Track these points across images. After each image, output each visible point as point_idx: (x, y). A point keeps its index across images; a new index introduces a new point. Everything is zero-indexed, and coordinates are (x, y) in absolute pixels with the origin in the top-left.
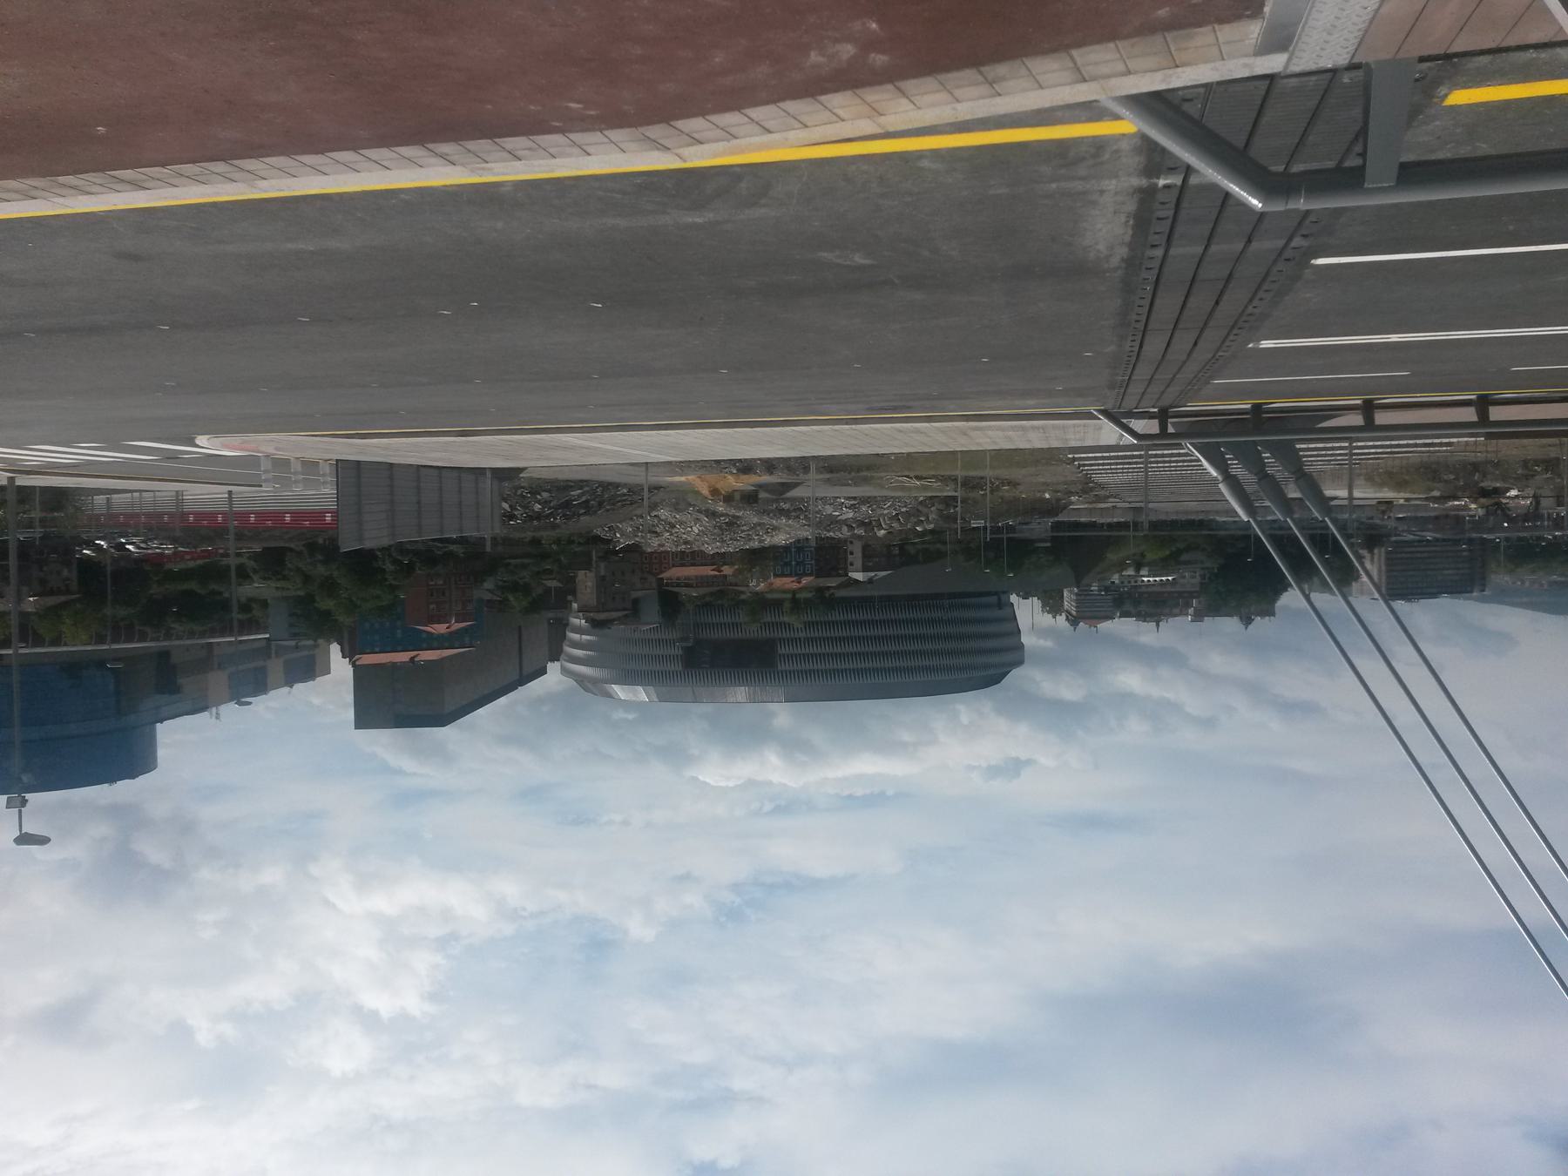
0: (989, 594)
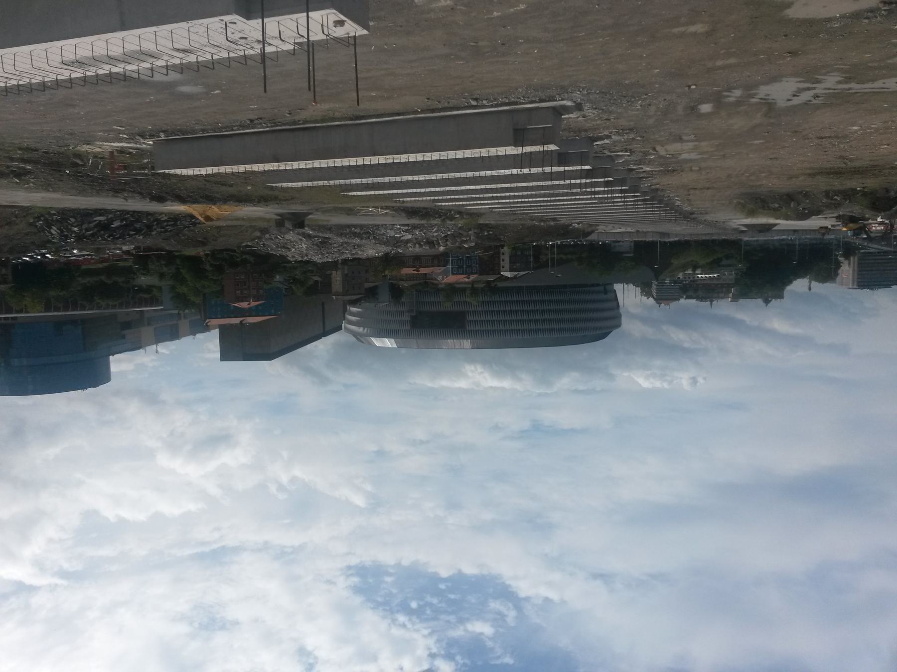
0: (598, 285)
